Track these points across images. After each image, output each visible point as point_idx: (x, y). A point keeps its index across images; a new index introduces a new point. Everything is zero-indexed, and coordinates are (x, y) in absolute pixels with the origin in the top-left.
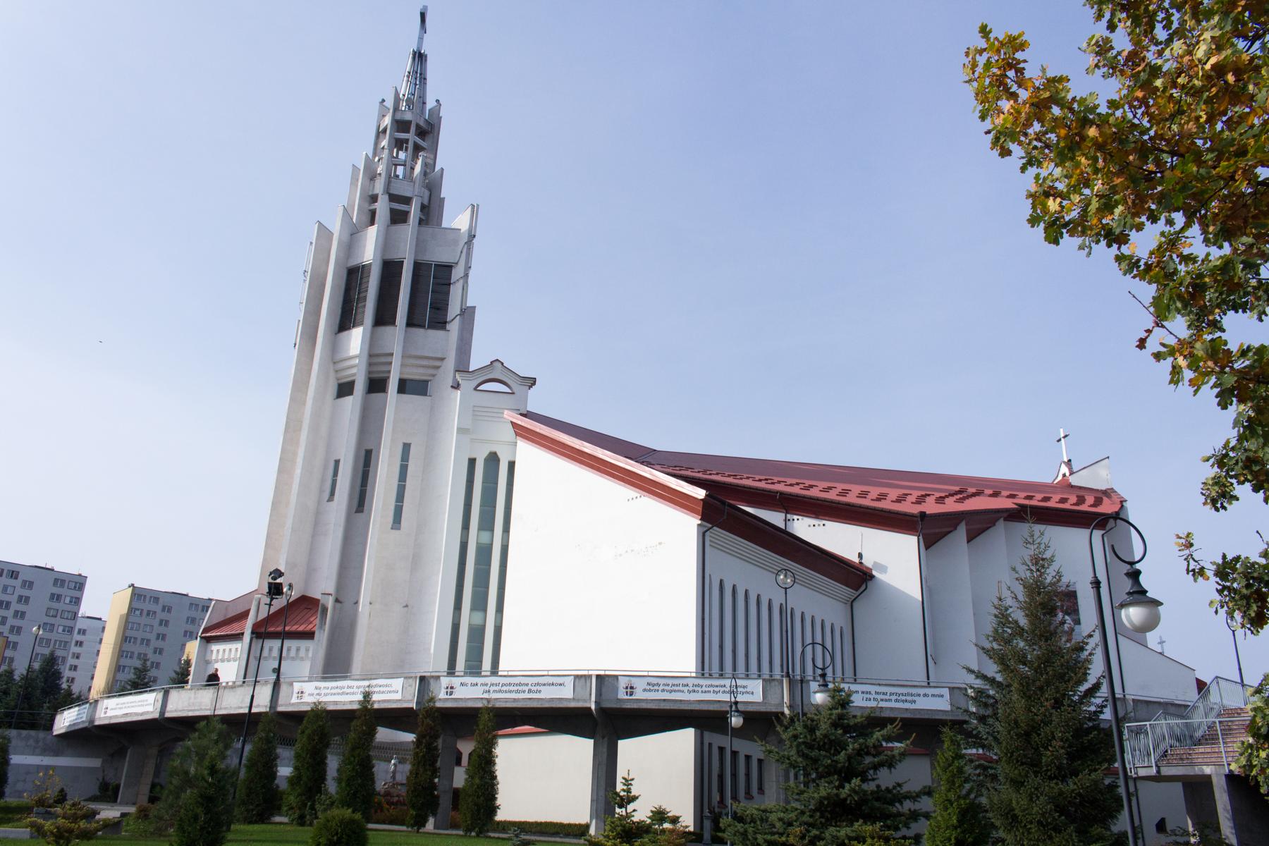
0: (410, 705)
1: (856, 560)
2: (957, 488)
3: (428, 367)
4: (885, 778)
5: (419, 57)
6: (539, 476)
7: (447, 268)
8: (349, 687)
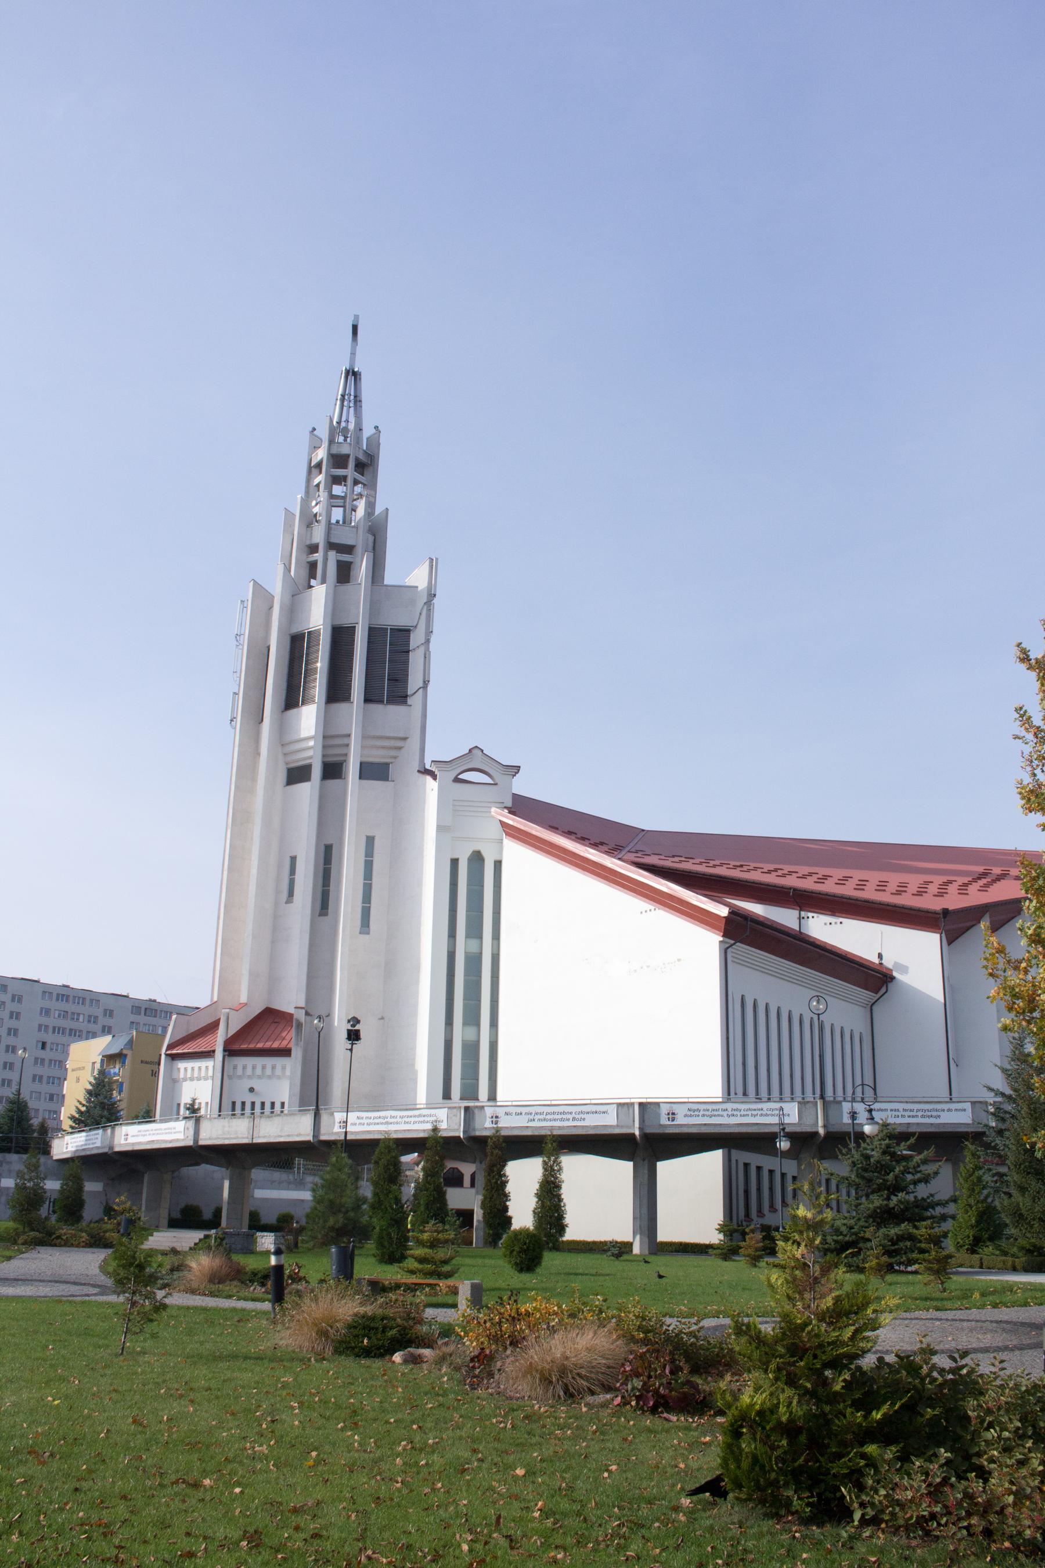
0: (456, 1134)
1: (876, 961)
2: (980, 869)
3: (390, 748)
4: (922, 1191)
5: (353, 374)
6: (535, 885)
7: (402, 634)
8: (392, 1117)
